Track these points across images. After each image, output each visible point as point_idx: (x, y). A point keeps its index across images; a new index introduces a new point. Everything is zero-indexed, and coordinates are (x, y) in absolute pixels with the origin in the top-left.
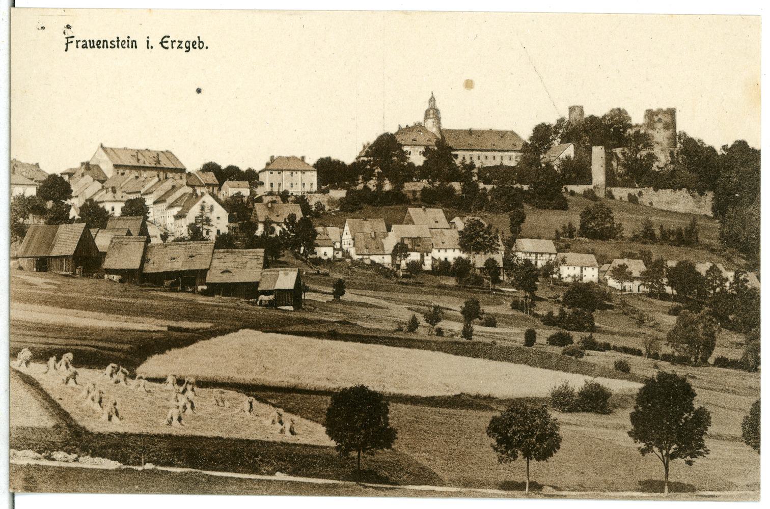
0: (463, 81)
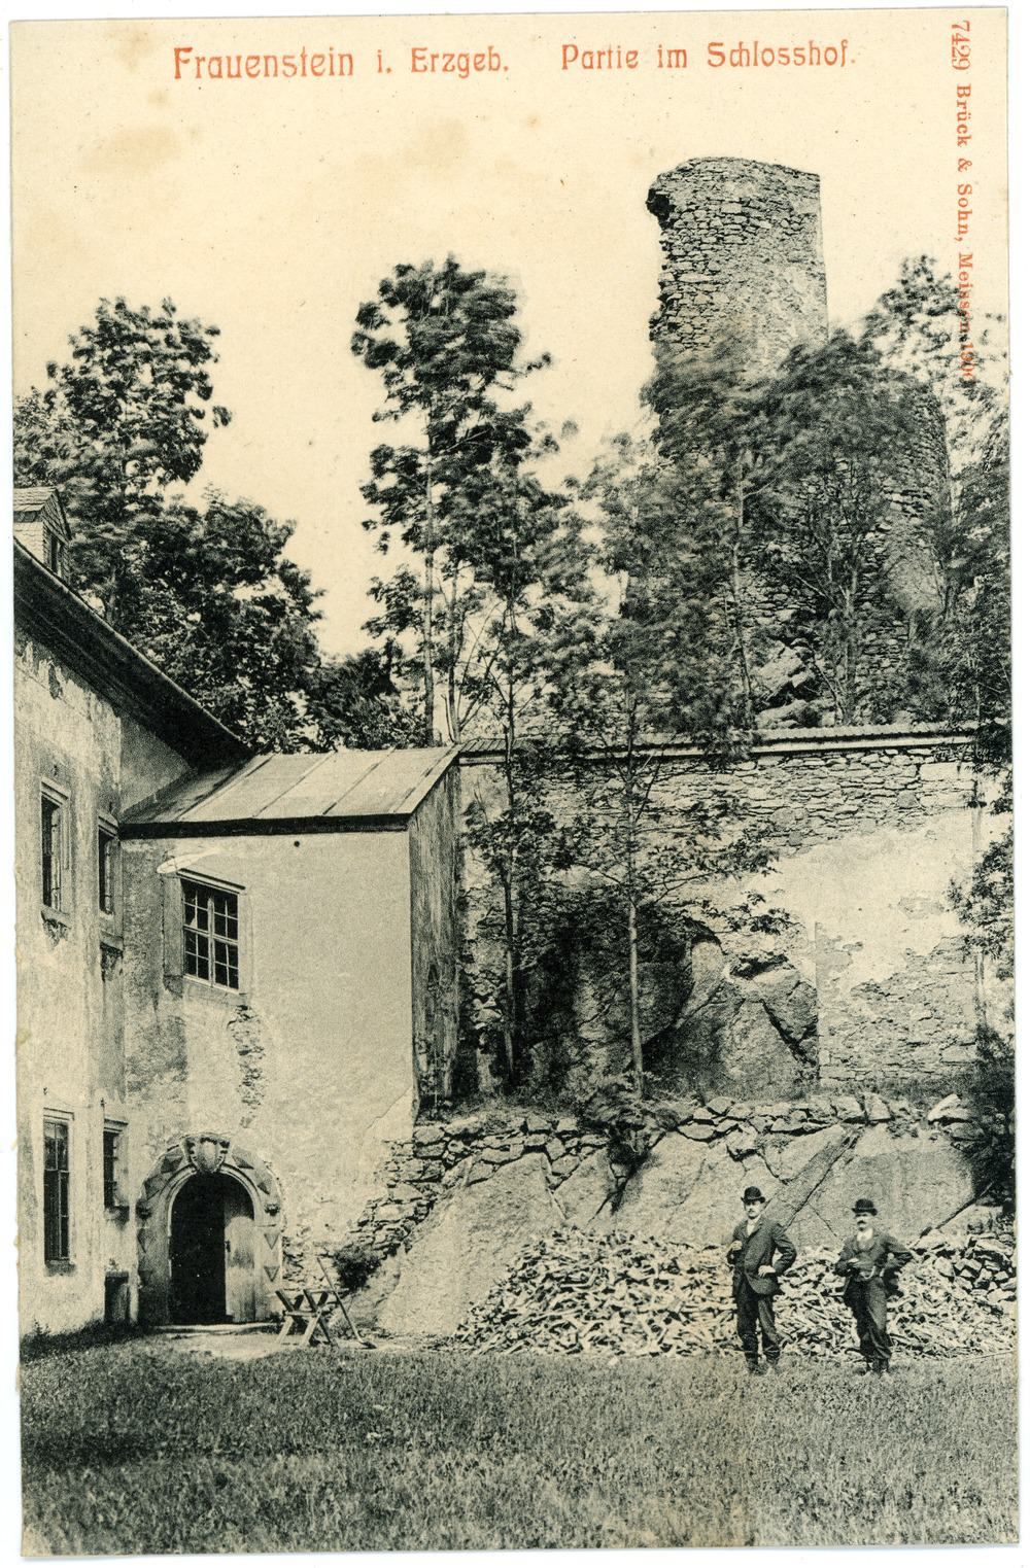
0: (577, 421)
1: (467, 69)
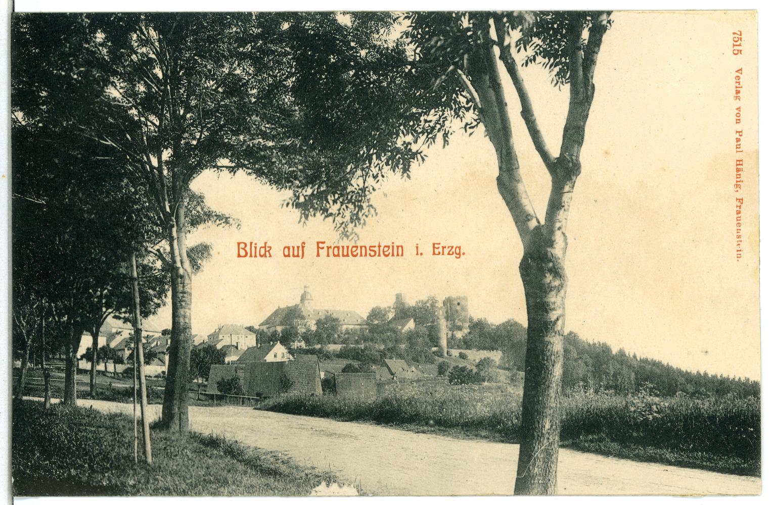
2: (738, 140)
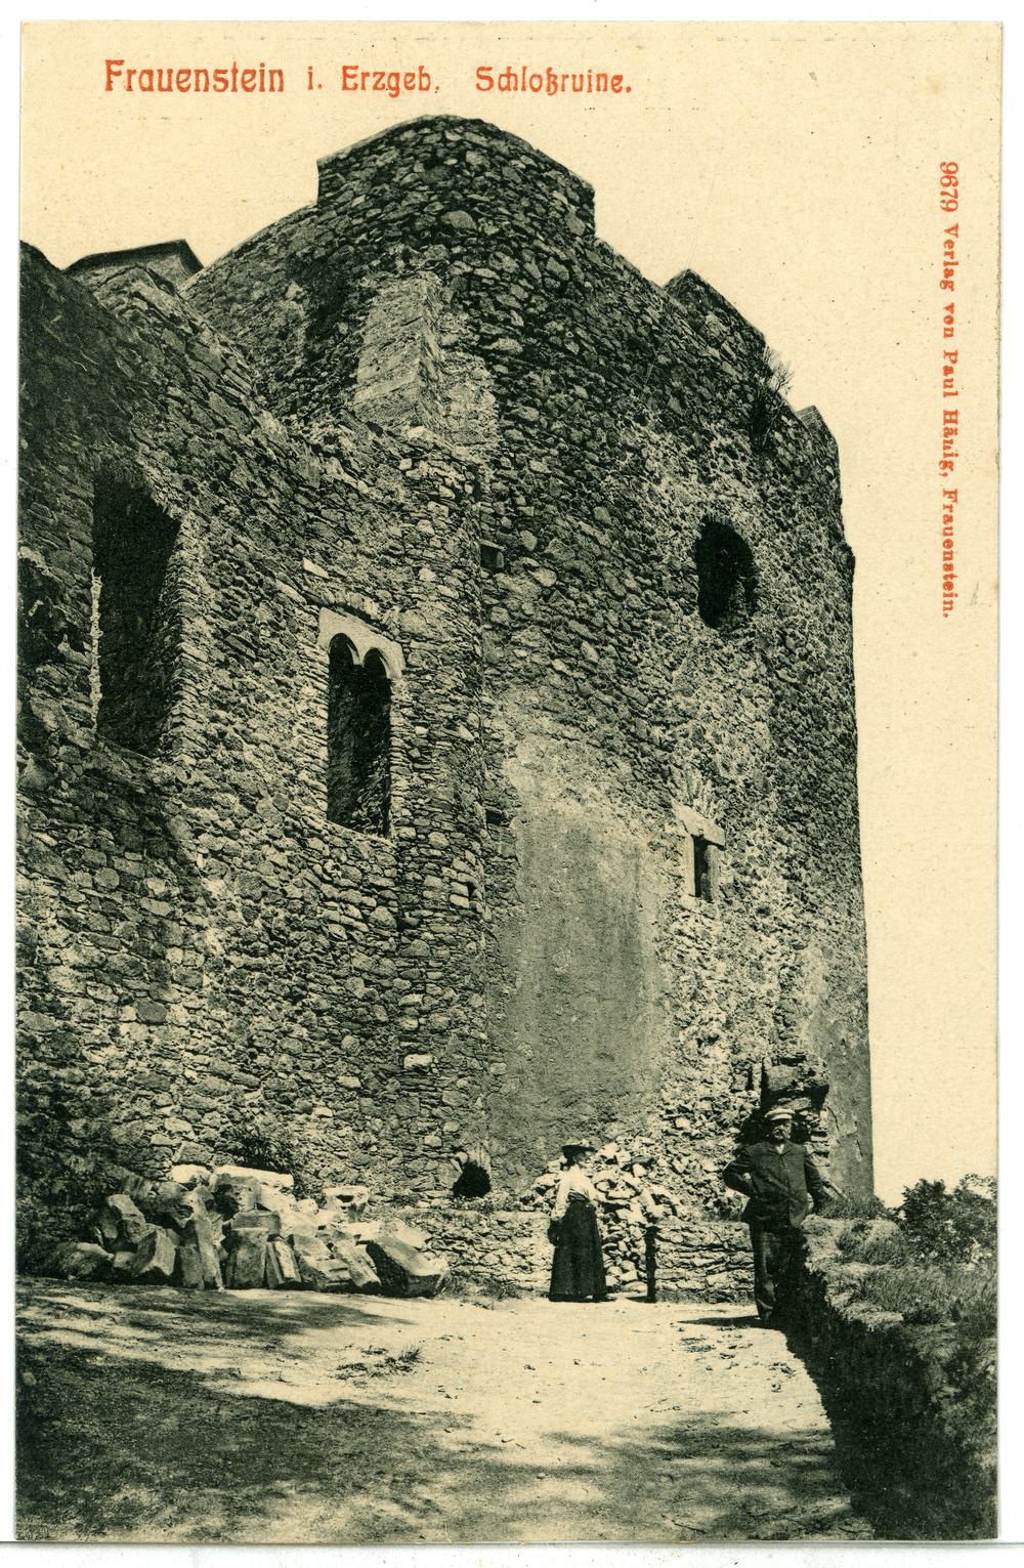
1: (397, 88)
2: (948, 370)
